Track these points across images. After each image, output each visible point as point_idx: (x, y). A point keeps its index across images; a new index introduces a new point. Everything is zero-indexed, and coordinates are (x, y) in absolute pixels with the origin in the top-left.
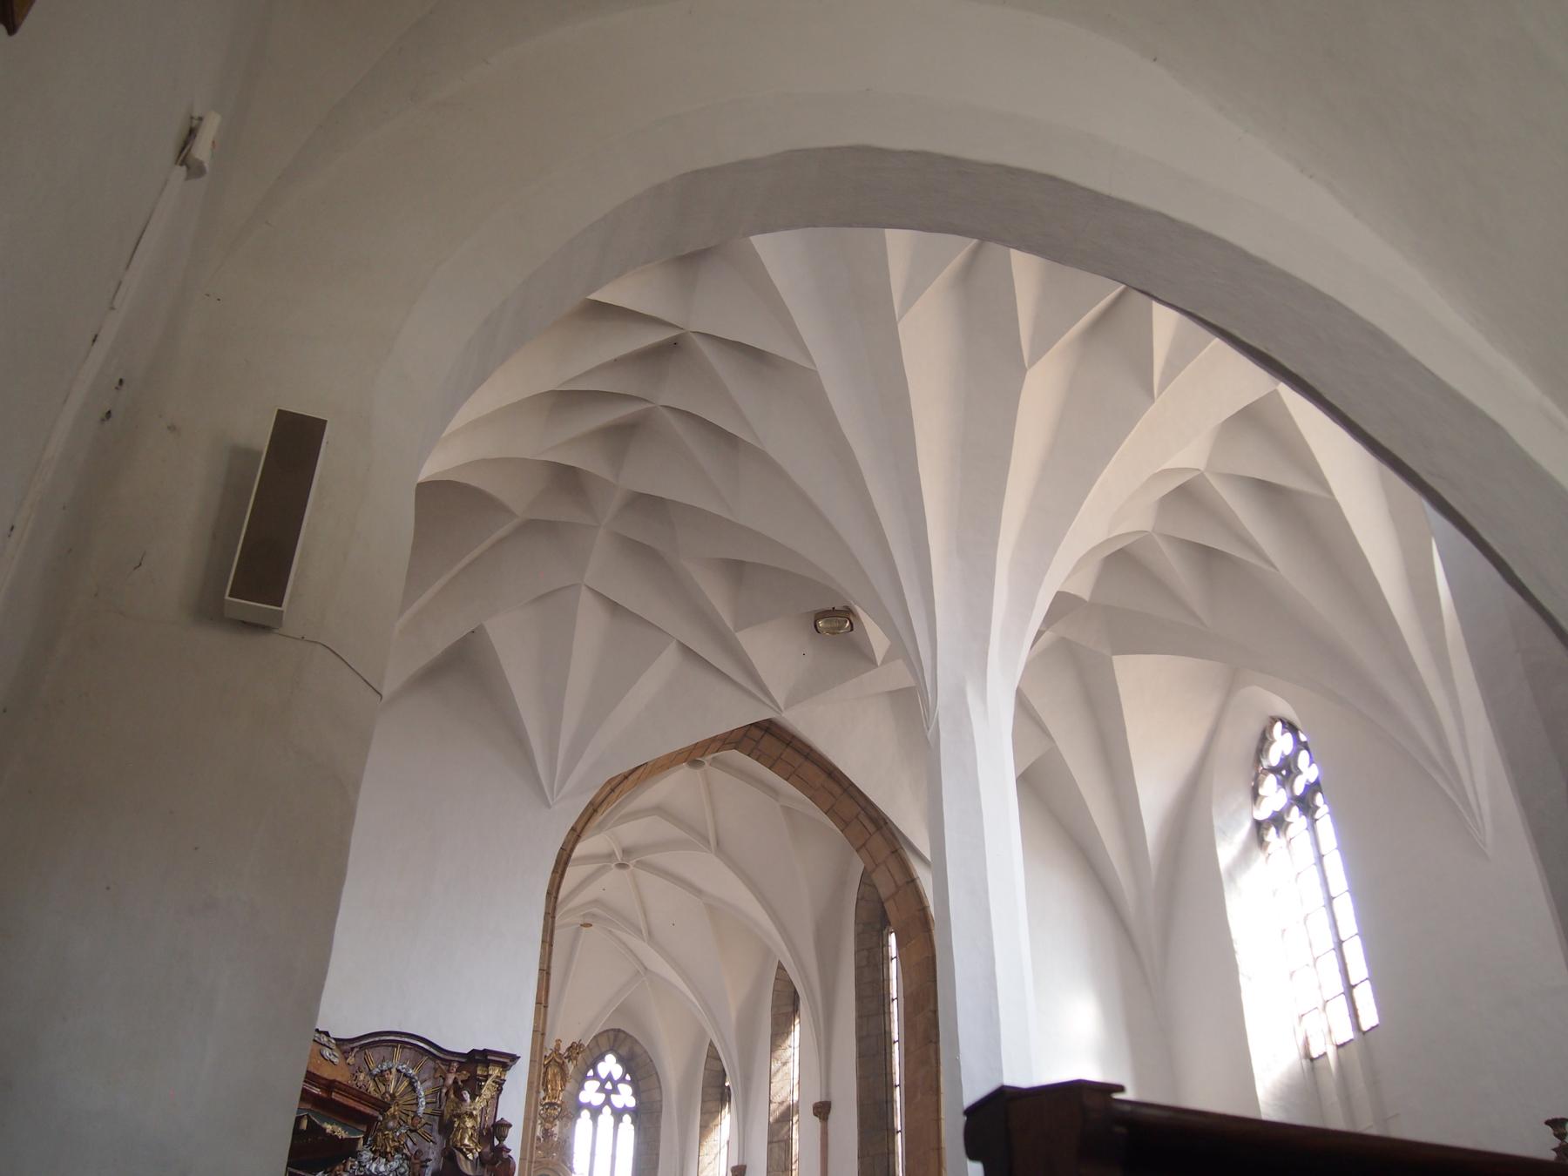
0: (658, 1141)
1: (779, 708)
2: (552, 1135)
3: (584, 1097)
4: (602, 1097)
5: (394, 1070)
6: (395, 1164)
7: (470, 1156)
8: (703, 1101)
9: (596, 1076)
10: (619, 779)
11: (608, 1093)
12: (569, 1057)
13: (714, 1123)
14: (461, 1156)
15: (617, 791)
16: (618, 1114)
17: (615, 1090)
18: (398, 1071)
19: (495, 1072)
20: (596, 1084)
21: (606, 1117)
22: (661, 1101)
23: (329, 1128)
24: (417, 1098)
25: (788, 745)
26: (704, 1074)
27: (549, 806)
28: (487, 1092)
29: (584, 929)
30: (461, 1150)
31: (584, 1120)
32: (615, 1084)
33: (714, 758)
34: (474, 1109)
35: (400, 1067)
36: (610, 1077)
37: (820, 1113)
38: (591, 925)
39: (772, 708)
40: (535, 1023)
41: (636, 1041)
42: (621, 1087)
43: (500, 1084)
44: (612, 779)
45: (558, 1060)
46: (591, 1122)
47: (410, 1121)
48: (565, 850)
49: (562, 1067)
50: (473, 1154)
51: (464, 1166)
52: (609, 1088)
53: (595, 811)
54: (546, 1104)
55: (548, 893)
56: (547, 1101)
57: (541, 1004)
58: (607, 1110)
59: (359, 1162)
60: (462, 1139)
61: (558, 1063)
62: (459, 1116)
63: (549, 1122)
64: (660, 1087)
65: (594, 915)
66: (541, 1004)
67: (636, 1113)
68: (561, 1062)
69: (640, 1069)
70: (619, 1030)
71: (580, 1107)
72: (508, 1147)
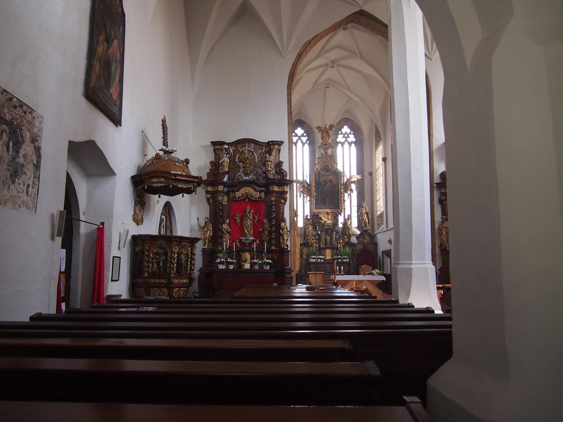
1: (360, 6)
2: (327, 153)
3: (338, 140)
4: (344, 139)
5: (246, 150)
6: (251, 177)
7: (271, 172)
8: (376, 137)
10: (307, 43)
11: (346, 138)
12: (330, 129)
13: (380, 144)
14: (268, 173)
15: (308, 48)
16: (350, 144)
17: (348, 137)
18: (248, 150)
19: (276, 147)
20: (342, 136)
21: (346, 145)
22: (363, 138)
23: (180, 186)
24: (255, 157)
25: (370, 18)
27: (284, 58)
28: (274, 153)
29: (327, 89)
30: (268, 171)
31: (339, 146)
33: (351, 25)
34: (270, 159)
35: (248, 149)
36: (346, 133)
37: (334, 162)
38: (329, 87)
39: (357, 6)
41: (353, 121)
43: (279, 151)
44: (305, 44)
45: (326, 131)
46: (342, 147)
47: (253, 164)
48: (291, 72)
49: (327, 132)
50: (272, 172)
51: (270, 176)
52: (346, 136)
53: (300, 56)
54: (324, 144)
55: (287, 87)
56: (324, 143)
58: (346, 143)
59: (241, 177)
60: (268, 168)
62: (266, 161)
64: (362, 134)
65: (329, 84)
67: (355, 143)
69: (356, 129)
71: (337, 143)
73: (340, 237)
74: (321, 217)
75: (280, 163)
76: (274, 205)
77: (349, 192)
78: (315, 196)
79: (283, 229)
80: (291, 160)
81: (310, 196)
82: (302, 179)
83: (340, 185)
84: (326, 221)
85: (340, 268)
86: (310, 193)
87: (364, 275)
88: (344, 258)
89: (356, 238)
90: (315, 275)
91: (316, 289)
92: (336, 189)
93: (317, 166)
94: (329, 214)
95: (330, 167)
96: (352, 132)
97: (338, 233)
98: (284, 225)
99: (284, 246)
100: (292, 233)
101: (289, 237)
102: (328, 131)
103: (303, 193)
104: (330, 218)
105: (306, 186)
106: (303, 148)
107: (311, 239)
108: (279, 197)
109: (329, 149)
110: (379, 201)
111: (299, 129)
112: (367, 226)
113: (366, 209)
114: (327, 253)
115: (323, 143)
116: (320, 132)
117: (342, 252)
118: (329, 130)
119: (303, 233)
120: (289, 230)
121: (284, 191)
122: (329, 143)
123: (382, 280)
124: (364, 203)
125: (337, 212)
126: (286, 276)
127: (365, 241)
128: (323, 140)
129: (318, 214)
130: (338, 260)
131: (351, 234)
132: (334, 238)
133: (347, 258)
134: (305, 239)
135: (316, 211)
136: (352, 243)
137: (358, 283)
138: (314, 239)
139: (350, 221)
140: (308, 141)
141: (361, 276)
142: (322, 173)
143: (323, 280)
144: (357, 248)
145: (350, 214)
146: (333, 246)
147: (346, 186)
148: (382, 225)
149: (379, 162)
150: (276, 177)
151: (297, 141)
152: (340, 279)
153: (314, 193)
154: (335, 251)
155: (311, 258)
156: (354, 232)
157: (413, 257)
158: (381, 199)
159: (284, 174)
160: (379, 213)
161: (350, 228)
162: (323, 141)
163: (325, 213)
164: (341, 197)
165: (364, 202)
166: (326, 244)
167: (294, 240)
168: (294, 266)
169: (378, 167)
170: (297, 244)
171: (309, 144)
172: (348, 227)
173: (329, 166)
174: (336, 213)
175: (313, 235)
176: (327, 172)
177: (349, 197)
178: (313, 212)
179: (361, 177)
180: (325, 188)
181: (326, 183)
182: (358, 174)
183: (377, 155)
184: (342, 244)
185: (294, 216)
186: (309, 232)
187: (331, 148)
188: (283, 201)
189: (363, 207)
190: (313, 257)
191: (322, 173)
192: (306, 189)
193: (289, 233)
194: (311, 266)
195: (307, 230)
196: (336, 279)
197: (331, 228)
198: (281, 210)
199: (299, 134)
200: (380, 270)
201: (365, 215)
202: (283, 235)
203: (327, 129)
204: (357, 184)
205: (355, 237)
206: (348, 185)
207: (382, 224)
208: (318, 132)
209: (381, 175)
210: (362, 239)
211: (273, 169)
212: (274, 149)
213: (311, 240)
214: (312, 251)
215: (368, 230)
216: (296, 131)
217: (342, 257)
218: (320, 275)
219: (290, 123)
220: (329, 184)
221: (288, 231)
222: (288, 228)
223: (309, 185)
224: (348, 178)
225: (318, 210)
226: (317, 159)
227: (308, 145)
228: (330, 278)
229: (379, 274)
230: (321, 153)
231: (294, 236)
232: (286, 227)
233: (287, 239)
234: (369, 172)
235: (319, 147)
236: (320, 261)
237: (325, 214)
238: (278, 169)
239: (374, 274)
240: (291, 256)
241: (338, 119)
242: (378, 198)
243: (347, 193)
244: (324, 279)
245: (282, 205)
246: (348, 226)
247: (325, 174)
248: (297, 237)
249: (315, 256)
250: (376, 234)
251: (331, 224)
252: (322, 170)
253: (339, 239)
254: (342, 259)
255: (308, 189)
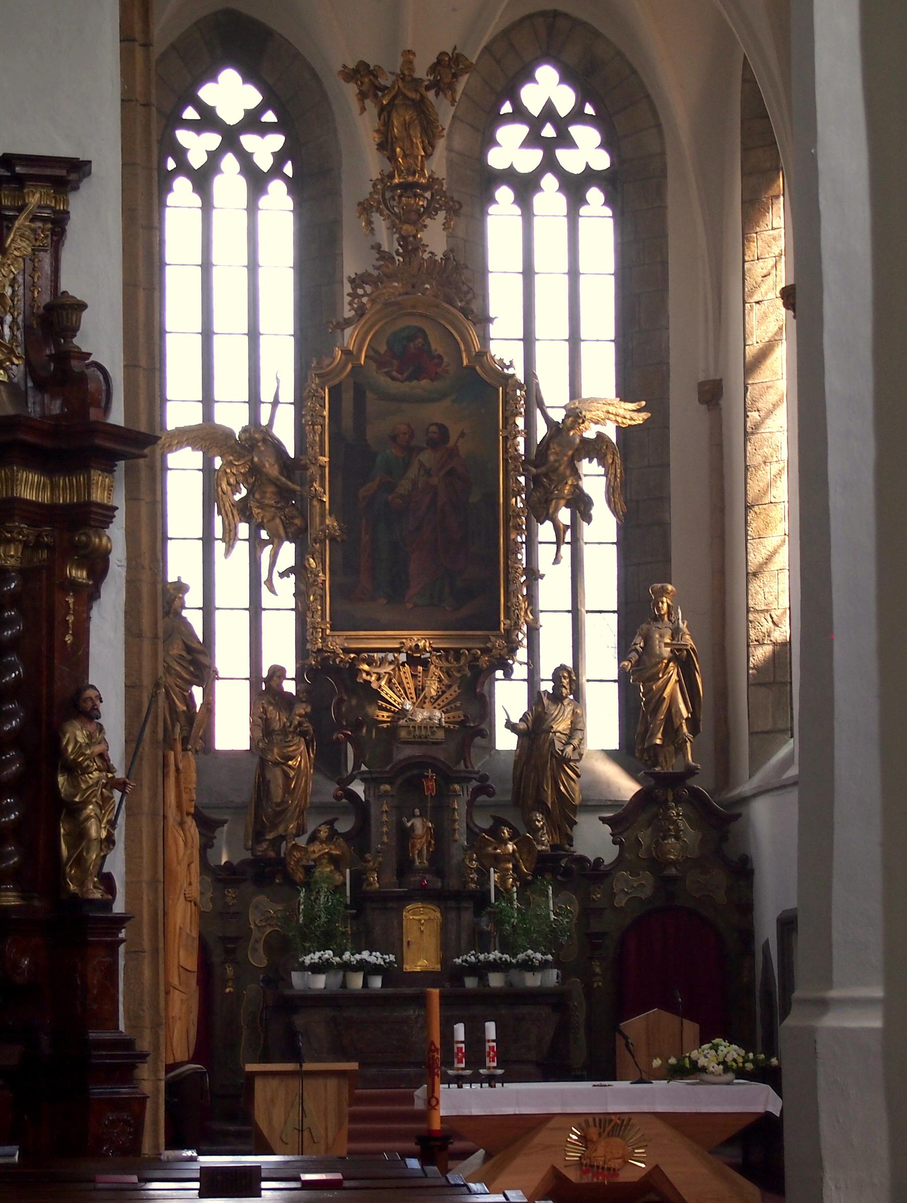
0: (664, 236)
2: (416, 249)
3: (497, 159)
8: (745, 149)
9: (520, 114)
11: (549, 146)
12: (437, 86)
13: (771, 193)
20: (520, 131)
22: (663, 153)
26: (742, 91)
32: (562, 125)
36: (549, 113)
40: (123, 83)
41: (597, 34)
42: (577, 131)
46: (517, 210)
49: (421, 108)
54: (400, 186)
57: (134, 40)
58: (549, 182)
61: (413, 100)
63: (407, 222)
64: (659, 126)
66: (134, 40)
68: (417, 97)
70: (556, 14)
72: (84, 350)
73: (499, 822)
74: (374, 685)
75: (63, 306)
76: (15, 599)
77: (564, 515)
78: (333, 539)
79: (74, 770)
80: (157, 294)
81: (299, 537)
82: (246, 422)
83: (505, 461)
84: (403, 712)
85: (475, 1037)
86: (297, 521)
87: (641, 1081)
88: (528, 966)
89: (607, 829)
90: (295, 1083)
91: (264, 1185)
92: (474, 498)
93: (349, 337)
94: (425, 663)
95: (434, 346)
96: (589, 110)
97: (491, 795)
98: (81, 738)
99: (82, 884)
100: (146, 793)
101: (121, 820)
102: (423, 97)
103: (248, 519)
104: (433, 689)
105: (272, 469)
106: (252, 209)
107: (300, 831)
108: (50, 548)
109: (428, 221)
110: (765, 577)
111: (230, 77)
112: (680, 749)
113: (676, 633)
114: (411, 933)
115: (391, 176)
116: (368, 103)
117: (514, 921)
118: (431, 95)
119: (245, 794)
120: (120, 774)
121: (90, 504)
122: (433, 180)
123: (760, 1109)
124: (664, 592)
125: (486, 651)
126: (99, 1091)
127: (673, 848)
128: (392, 158)
129: (353, 664)
130: (483, 979)
131: (577, 799)
132: (461, 826)
133: (544, 965)
134: (258, 836)
135: (337, 642)
136: (582, 859)
137: (593, 1132)
138: (323, 834)
139: (569, 709)
140: (289, 164)
141: (616, 1084)
142: (383, 380)
143: (354, 1118)
144: (614, 895)
145: (569, 664)
146: (454, 883)
147: (546, 475)
148: (786, 742)
149: (765, 316)
150: (33, 409)
151: (214, 158)
152: (475, 1112)
153: (323, 516)
154: (467, 916)
155: (303, 968)
156: (597, 783)
157: (836, 975)
158: (774, 566)
159: (91, 386)
160: (761, 654)
161: (567, 761)
162: (388, 167)
163: (403, 657)
164: (511, 550)
165: (331, 630)
166: (404, 867)
167: (161, 839)
168: (156, 1025)
169: (757, 347)
170: (181, 870)
171: (295, 186)
172: (554, 754)
173: (431, 339)
174: (476, 658)
175: (321, 808)
176: (416, 375)
177: (566, 550)
178: (320, 651)
179: (644, 415)
180: (404, 486)
181: (411, 451)
182: (625, 392)
183: (757, 269)
184: (516, 868)
185: (155, 669)
186: (287, 789)
187: (442, 215)
188: (80, 575)
189: (658, 618)
190: (314, 957)
191: (383, 380)
192: (271, 489)
193: (117, 794)
194: (299, 1021)
195: (278, 772)
196: (443, 1113)
197: (441, 756)
198: (69, 639)
199: (231, 115)
200: (747, 1044)
201: (673, 672)
202: (74, 811)
203: (416, 83)
204: (618, 461)
205: (604, 820)
206: (555, 470)
207: (783, 731)
208: (355, 105)
209: (775, 406)
210: (649, 831)
211: (11, 351)
212: (20, 209)
213: (302, 841)
214: (311, 918)
215: (691, 772)
216: (208, 93)
217: (514, 956)
218: (332, 1083)
219: (138, 35)
220: (427, 457)
221: (113, 784)
222: (117, 755)
223: (287, 465)
224: (558, 416)
225: (347, 638)
226: (347, 288)
227: (290, 192)
228: (410, 1099)
229: (741, 1074)
230: (378, 247)
231: (154, 814)
232: (103, 756)
233: (104, 834)
234: (702, 378)
235: (365, 208)
236: (365, 984)
237: (399, 665)
238: (50, 351)
239: (704, 1070)
240: (134, 954)
241: (497, 19)
242: (754, 559)
243: (548, 524)
244: (356, 1108)
245: (71, 601)
246: (558, 746)
247: (395, 387)
248: (182, 824)
249: (328, 954)
250: (745, 800)
251: (440, 735)
252: (381, 364)
253: (494, 832)
254: (514, 974)
255: (284, 494)
